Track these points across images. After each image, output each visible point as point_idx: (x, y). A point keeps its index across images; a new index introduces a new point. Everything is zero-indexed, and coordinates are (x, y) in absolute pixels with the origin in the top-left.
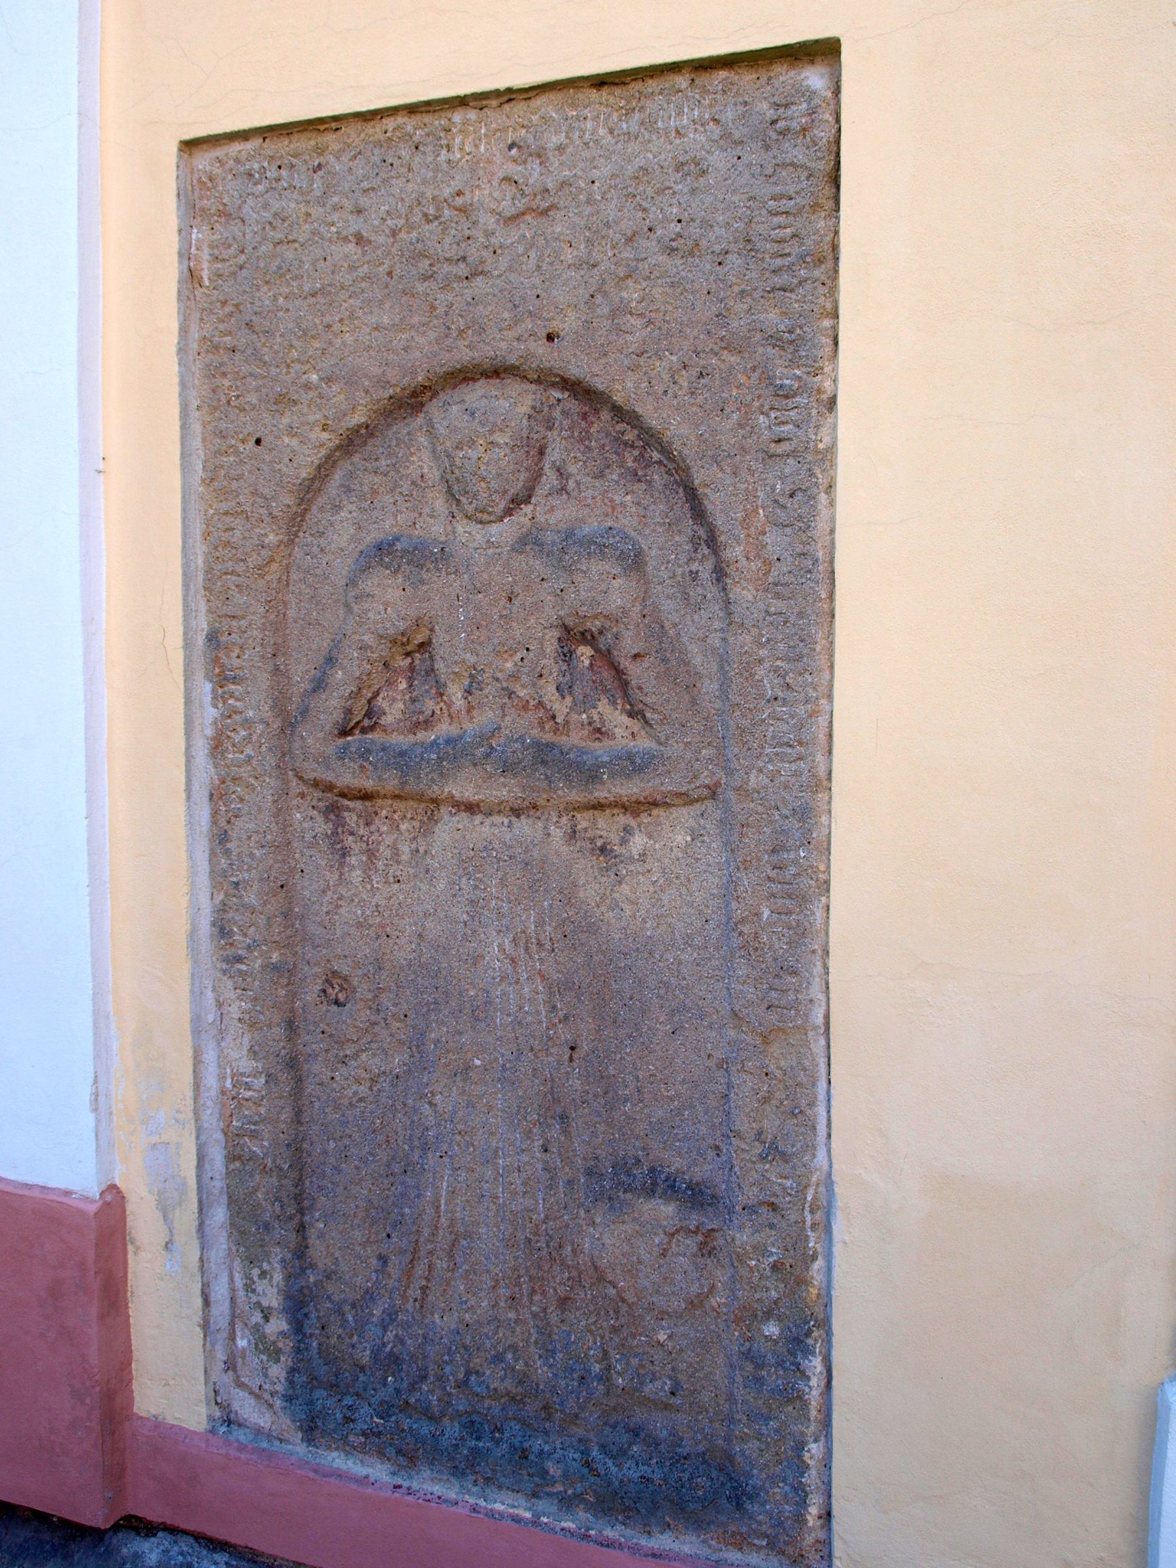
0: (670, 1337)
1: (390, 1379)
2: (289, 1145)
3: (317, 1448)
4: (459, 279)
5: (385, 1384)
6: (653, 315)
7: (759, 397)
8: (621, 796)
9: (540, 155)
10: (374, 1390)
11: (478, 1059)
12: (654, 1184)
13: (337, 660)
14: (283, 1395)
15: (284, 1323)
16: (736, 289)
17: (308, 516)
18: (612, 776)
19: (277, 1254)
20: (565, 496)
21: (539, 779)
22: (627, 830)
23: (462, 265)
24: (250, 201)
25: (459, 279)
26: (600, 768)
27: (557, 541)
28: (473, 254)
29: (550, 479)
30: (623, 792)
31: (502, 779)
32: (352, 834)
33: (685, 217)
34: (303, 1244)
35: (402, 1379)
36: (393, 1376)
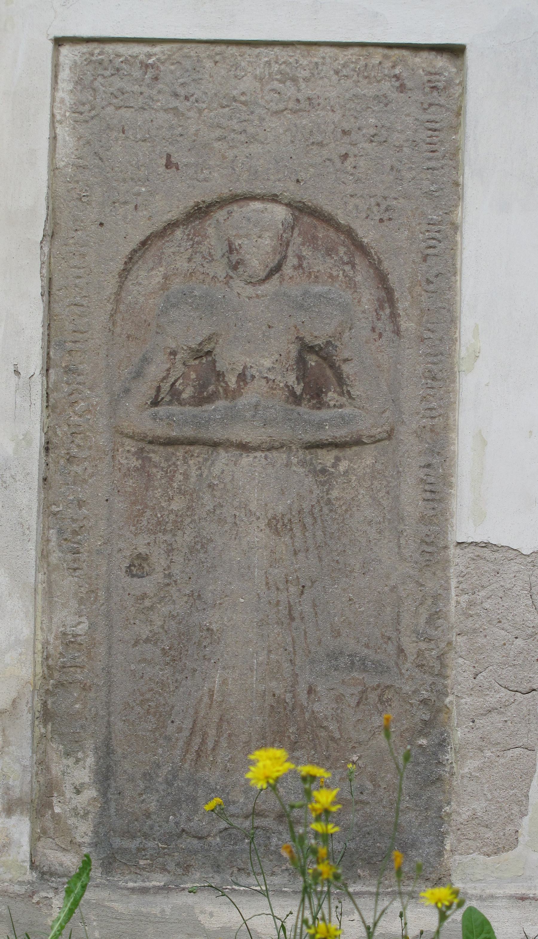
0: (360, 757)
1: (171, 817)
2: (103, 669)
3: (113, 877)
4: (242, 143)
5: (167, 822)
6: (360, 175)
7: (420, 224)
8: (336, 438)
9: (294, 80)
10: (159, 826)
11: (242, 598)
12: (353, 663)
13: (152, 359)
14: (89, 844)
15: (94, 791)
16: (407, 166)
17: (131, 272)
18: (331, 426)
19: (90, 744)
20: (301, 271)
21: (286, 429)
22: (338, 459)
23: (244, 135)
24: (100, 79)
25: (242, 143)
26: (323, 422)
27: (299, 295)
28: (251, 130)
29: (292, 261)
30: (337, 435)
31: (263, 430)
32: (156, 467)
33: (379, 125)
34: (109, 737)
35: (181, 815)
36: (174, 815)
